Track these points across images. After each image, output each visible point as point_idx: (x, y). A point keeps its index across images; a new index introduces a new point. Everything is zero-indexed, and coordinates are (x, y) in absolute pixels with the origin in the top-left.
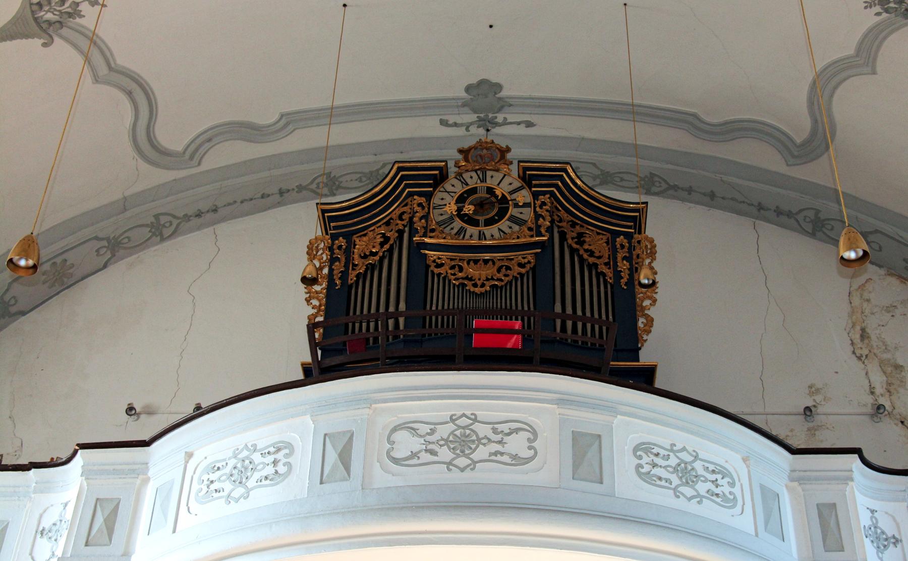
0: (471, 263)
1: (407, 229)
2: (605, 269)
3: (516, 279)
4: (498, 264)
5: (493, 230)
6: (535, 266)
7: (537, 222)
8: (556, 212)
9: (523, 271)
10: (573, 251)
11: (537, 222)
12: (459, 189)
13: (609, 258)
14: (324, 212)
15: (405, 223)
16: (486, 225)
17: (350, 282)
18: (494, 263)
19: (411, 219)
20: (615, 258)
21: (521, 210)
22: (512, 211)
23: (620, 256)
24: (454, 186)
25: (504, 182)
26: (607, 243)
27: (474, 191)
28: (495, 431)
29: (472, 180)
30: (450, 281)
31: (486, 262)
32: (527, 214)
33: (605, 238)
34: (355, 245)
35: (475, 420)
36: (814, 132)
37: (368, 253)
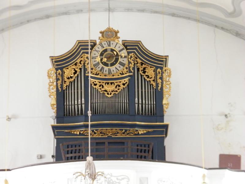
0: (106, 84)
1: (83, 67)
2: (152, 82)
3: (122, 90)
4: (116, 84)
5: (113, 68)
6: (128, 84)
7: (129, 66)
8: (136, 60)
9: (125, 87)
10: (141, 76)
11: (129, 66)
12: (101, 50)
13: (154, 78)
14: (52, 59)
15: (82, 65)
16: (111, 66)
17: (64, 89)
18: (114, 84)
19: (84, 63)
20: (157, 78)
21: (123, 59)
22: (120, 60)
23: (158, 77)
24: (99, 48)
25: (117, 45)
26: (154, 71)
27: (106, 51)
28: (117, 179)
29: (106, 46)
30: (99, 92)
31: (111, 83)
32: (125, 61)
33: (153, 69)
34: (64, 73)
35: (112, 176)
36: (235, 10)
37: (70, 77)
